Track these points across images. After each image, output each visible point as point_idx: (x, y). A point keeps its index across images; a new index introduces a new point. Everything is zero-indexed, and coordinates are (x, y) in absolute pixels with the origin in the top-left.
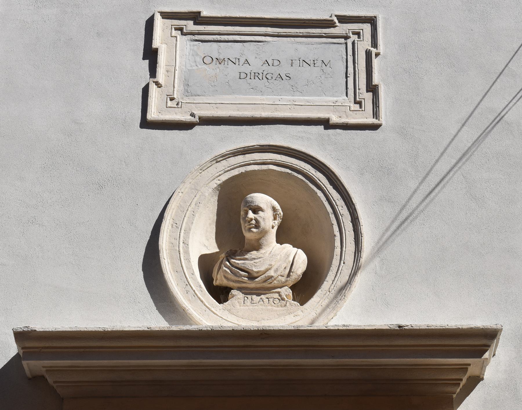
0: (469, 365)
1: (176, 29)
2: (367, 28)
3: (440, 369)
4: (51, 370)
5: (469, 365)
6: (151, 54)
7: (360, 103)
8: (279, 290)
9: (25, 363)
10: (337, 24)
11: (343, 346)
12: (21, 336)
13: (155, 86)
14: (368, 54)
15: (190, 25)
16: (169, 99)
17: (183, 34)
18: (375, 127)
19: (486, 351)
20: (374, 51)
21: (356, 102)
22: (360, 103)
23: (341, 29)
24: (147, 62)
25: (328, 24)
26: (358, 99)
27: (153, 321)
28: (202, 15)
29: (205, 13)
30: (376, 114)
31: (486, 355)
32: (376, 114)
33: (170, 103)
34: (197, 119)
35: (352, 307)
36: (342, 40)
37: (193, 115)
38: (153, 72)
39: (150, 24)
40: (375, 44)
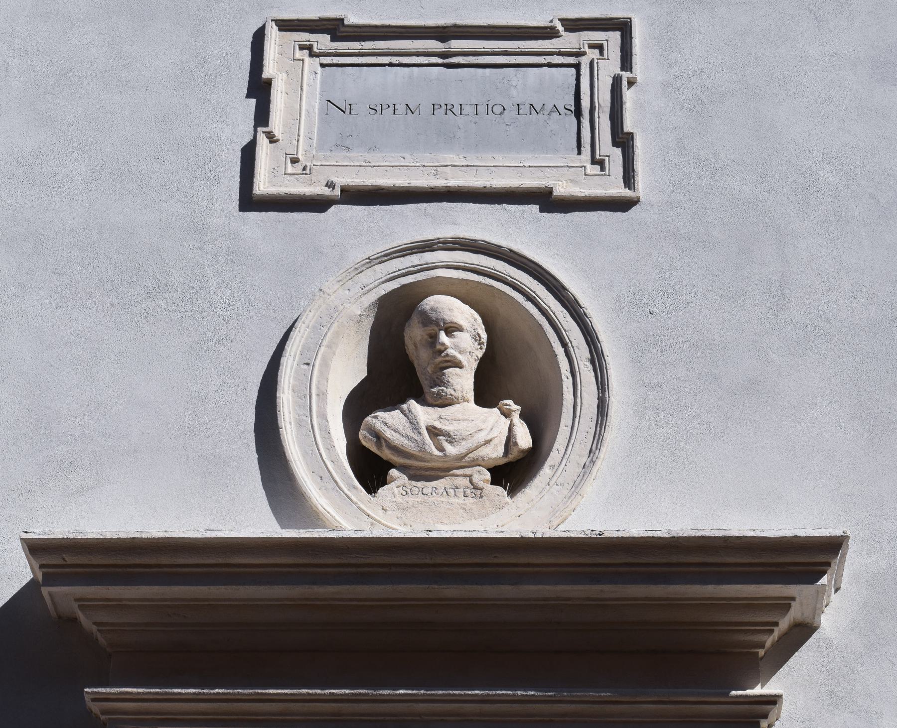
0: (793, 599)
1: (302, 48)
2: (614, 38)
3: (752, 605)
4: (85, 604)
5: (793, 599)
6: (260, 89)
7: (601, 163)
8: (468, 471)
9: (45, 591)
10: (563, 33)
11: (188, 566)
12: (36, 549)
13: (266, 141)
14: (616, 83)
15: (322, 41)
16: (289, 162)
17: (312, 55)
18: (622, 205)
19: (824, 573)
20: (626, 75)
21: (594, 161)
22: (601, 163)
23: (569, 41)
24: (253, 102)
25: (548, 33)
26: (598, 157)
27: (256, 521)
28: (346, 22)
29: (352, 19)
30: (629, 179)
31: (824, 580)
32: (629, 179)
33: (290, 169)
34: (337, 192)
35: (590, 497)
36: (572, 60)
37: (330, 185)
38: (262, 117)
39: (259, 38)
40: (626, 62)
